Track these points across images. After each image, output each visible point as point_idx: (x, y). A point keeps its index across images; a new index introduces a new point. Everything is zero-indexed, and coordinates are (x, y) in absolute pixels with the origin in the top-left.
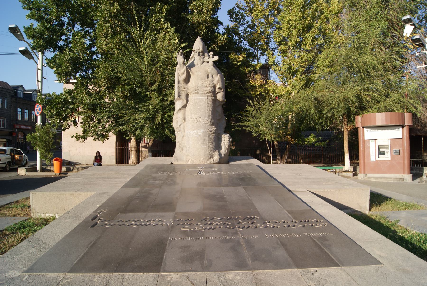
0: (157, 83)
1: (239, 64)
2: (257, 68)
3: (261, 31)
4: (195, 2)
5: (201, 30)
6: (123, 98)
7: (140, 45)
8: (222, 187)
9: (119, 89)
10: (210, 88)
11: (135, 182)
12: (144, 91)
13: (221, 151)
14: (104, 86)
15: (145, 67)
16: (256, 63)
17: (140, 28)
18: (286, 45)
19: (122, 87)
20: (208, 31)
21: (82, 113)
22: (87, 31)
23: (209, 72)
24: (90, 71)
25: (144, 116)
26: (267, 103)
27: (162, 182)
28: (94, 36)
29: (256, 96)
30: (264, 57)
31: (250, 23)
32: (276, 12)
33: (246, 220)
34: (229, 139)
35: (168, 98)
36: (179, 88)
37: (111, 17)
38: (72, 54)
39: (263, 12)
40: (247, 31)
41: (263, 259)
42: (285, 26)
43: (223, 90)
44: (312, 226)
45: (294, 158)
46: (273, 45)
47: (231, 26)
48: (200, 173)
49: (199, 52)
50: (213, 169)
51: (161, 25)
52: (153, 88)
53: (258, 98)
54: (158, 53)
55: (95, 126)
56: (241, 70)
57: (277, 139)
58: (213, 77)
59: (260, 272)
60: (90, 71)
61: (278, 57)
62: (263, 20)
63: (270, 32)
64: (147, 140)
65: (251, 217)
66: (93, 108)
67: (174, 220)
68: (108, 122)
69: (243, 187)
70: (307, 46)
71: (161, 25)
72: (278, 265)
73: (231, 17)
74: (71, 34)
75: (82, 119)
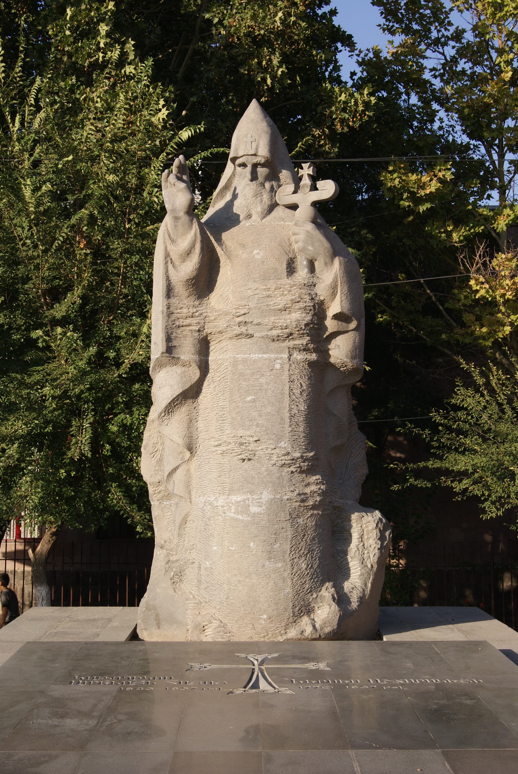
0: (78, 291)
1: (422, 208)
2: (501, 224)
5: (265, 70)
8: (352, 753)
10: (298, 317)
12: (20, 322)
13: (347, 586)
15: (25, 225)
16: (495, 202)
20: (291, 73)
23: (296, 247)
27: (93, 723)
29: (497, 345)
31: (469, 37)
34: (382, 533)
35: (123, 352)
36: (169, 313)
40: (455, 73)
43: (353, 325)
47: (386, 54)
48: (256, 686)
49: (255, 166)
50: (311, 666)
51: (99, 49)
52: (60, 311)
53: (504, 353)
54: (82, 166)
56: (432, 237)
58: (312, 268)
69: (445, 754)
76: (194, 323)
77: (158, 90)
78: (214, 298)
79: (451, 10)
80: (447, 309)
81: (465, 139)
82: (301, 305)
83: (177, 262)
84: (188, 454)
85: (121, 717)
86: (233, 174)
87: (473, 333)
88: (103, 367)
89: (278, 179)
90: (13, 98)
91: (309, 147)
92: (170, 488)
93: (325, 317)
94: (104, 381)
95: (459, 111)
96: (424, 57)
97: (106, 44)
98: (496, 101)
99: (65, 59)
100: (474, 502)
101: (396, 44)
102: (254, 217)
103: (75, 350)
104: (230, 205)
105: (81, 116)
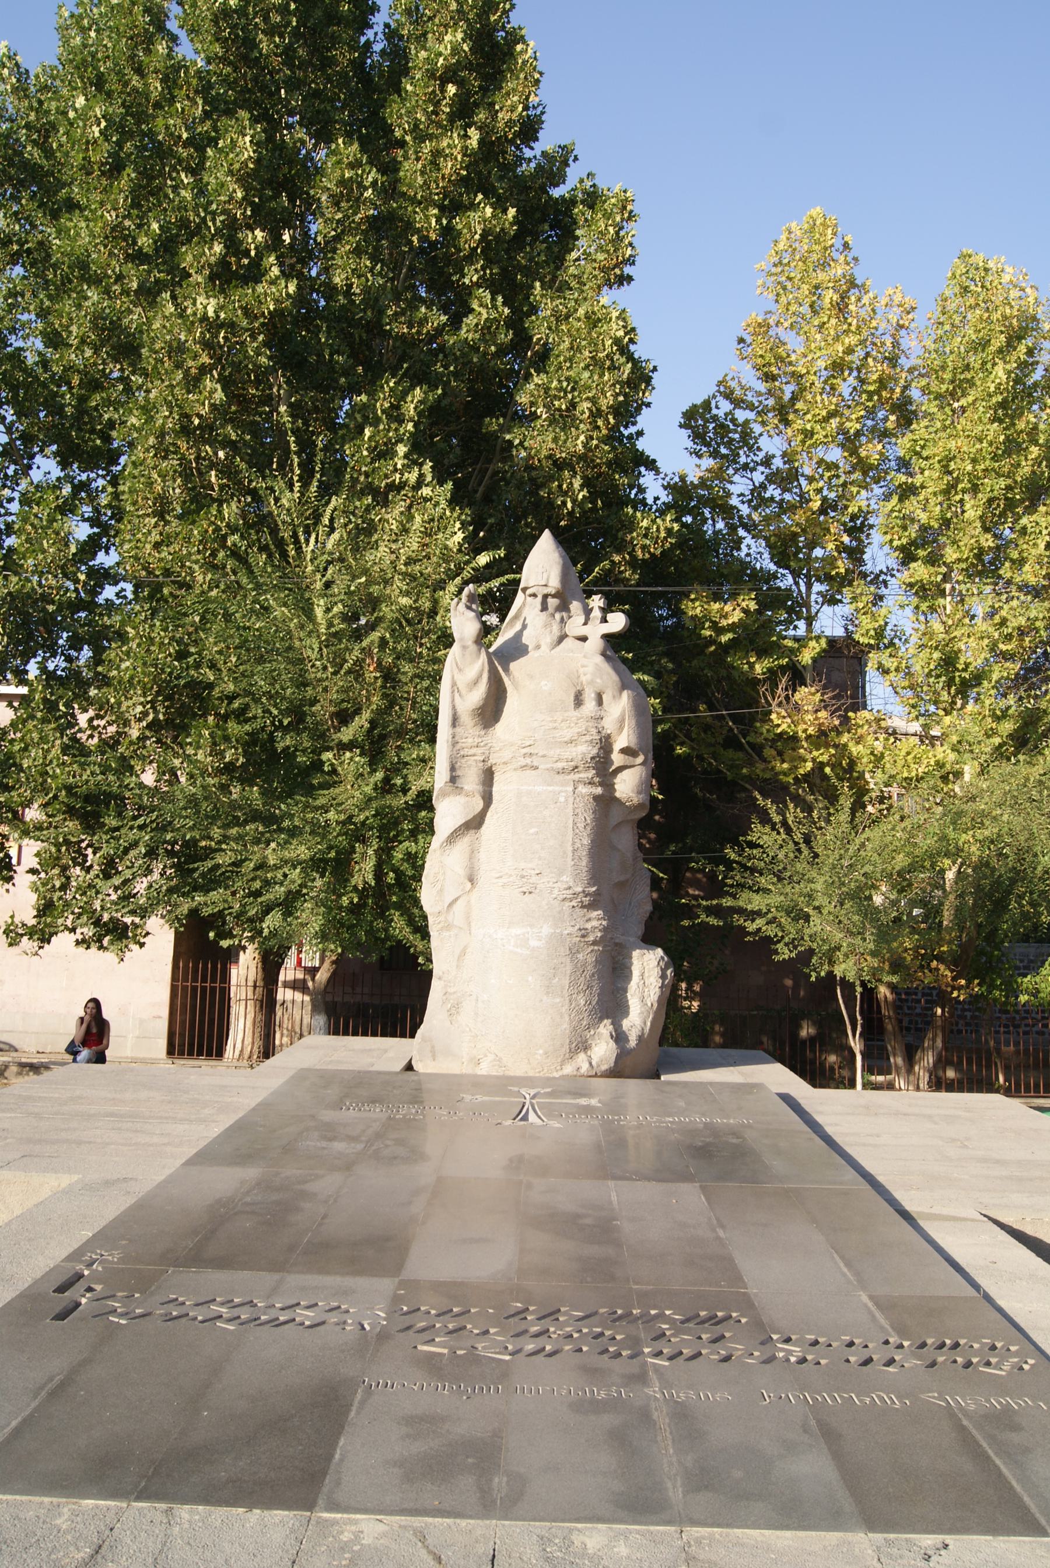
2: (806, 657)
3: (824, 499)
4: (543, 376)
5: (565, 494)
6: (219, 772)
7: (299, 549)
8: (611, 1183)
9: (200, 736)
10: (585, 750)
11: (242, 1142)
13: (626, 1024)
14: (140, 720)
15: (316, 646)
17: (306, 480)
18: (933, 560)
19: (217, 726)
20: (592, 498)
21: (39, 827)
22: (84, 486)
23: (584, 679)
24: (86, 653)
25: (301, 851)
26: (844, 816)
27: (360, 1147)
28: (109, 506)
30: (838, 608)
31: (778, 463)
32: (893, 418)
33: (691, 1325)
35: (410, 778)
37: (185, 430)
38: (14, 579)
39: (834, 422)
41: (735, 1488)
42: (930, 479)
43: (640, 759)
44: (968, 1364)
45: (970, 1062)
46: (879, 555)
47: (693, 478)
48: (525, 1118)
49: (545, 596)
50: (583, 1101)
51: (396, 470)
52: (346, 734)
54: (375, 590)
55: (90, 886)
57: (887, 978)
58: (600, 701)
59: (711, 1537)
60: (86, 653)
61: (899, 613)
62: (835, 454)
63: (863, 504)
64: (309, 958)
65: (718, 1314)
66: (90, 808)
67: (392, 1312)
68: (149, 871)
69: (703, 1189)
70: (1027, 568)
71: (396, 470)
72: (793, 1512)
73: (698, 436)
74: (16, 495)
75: (38, 855)
76: (479, 754)
77: (455, 515)
78: (500, 727)
79: (761, 435)
80: (748, 743)
81: (773, 567)
82: (588, 738)
83: (463, 692)
84: (469, 885)
85: (389, 1142)
86: (524, 604)
87: (773, 768)
88: (389, 792)
89: (568, 610)
90: (307, 519)
91: (608, 573)
92: (450, 919)
93: (611, 751)
94: (390, 807)
95: (767, 539)
96: (731, 483)
97: (403, 465)
98: (804, 530)
99: (362, 478)
100: (767, 943)
101: (703, 468)
102: (544, 647)
103: (362, 775)
104: (519, 635)
105: (375, 537)
